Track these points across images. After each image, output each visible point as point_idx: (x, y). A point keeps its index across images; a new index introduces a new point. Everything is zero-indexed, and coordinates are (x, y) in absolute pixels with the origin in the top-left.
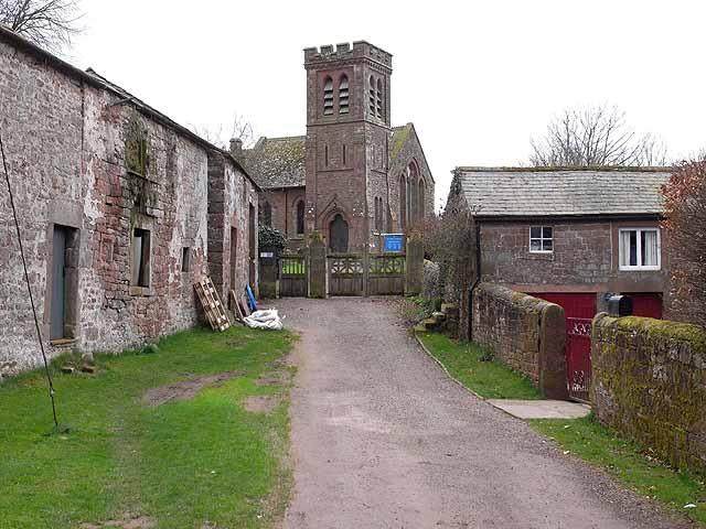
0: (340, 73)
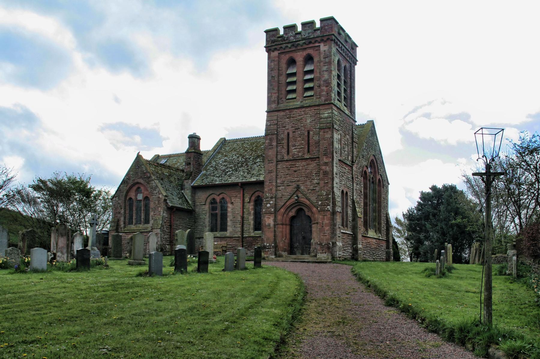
0: (305, 53)
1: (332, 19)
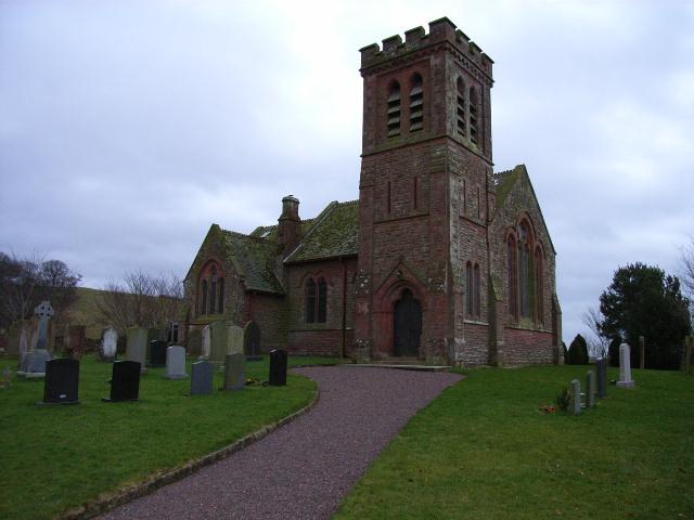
1: (445, 20)
